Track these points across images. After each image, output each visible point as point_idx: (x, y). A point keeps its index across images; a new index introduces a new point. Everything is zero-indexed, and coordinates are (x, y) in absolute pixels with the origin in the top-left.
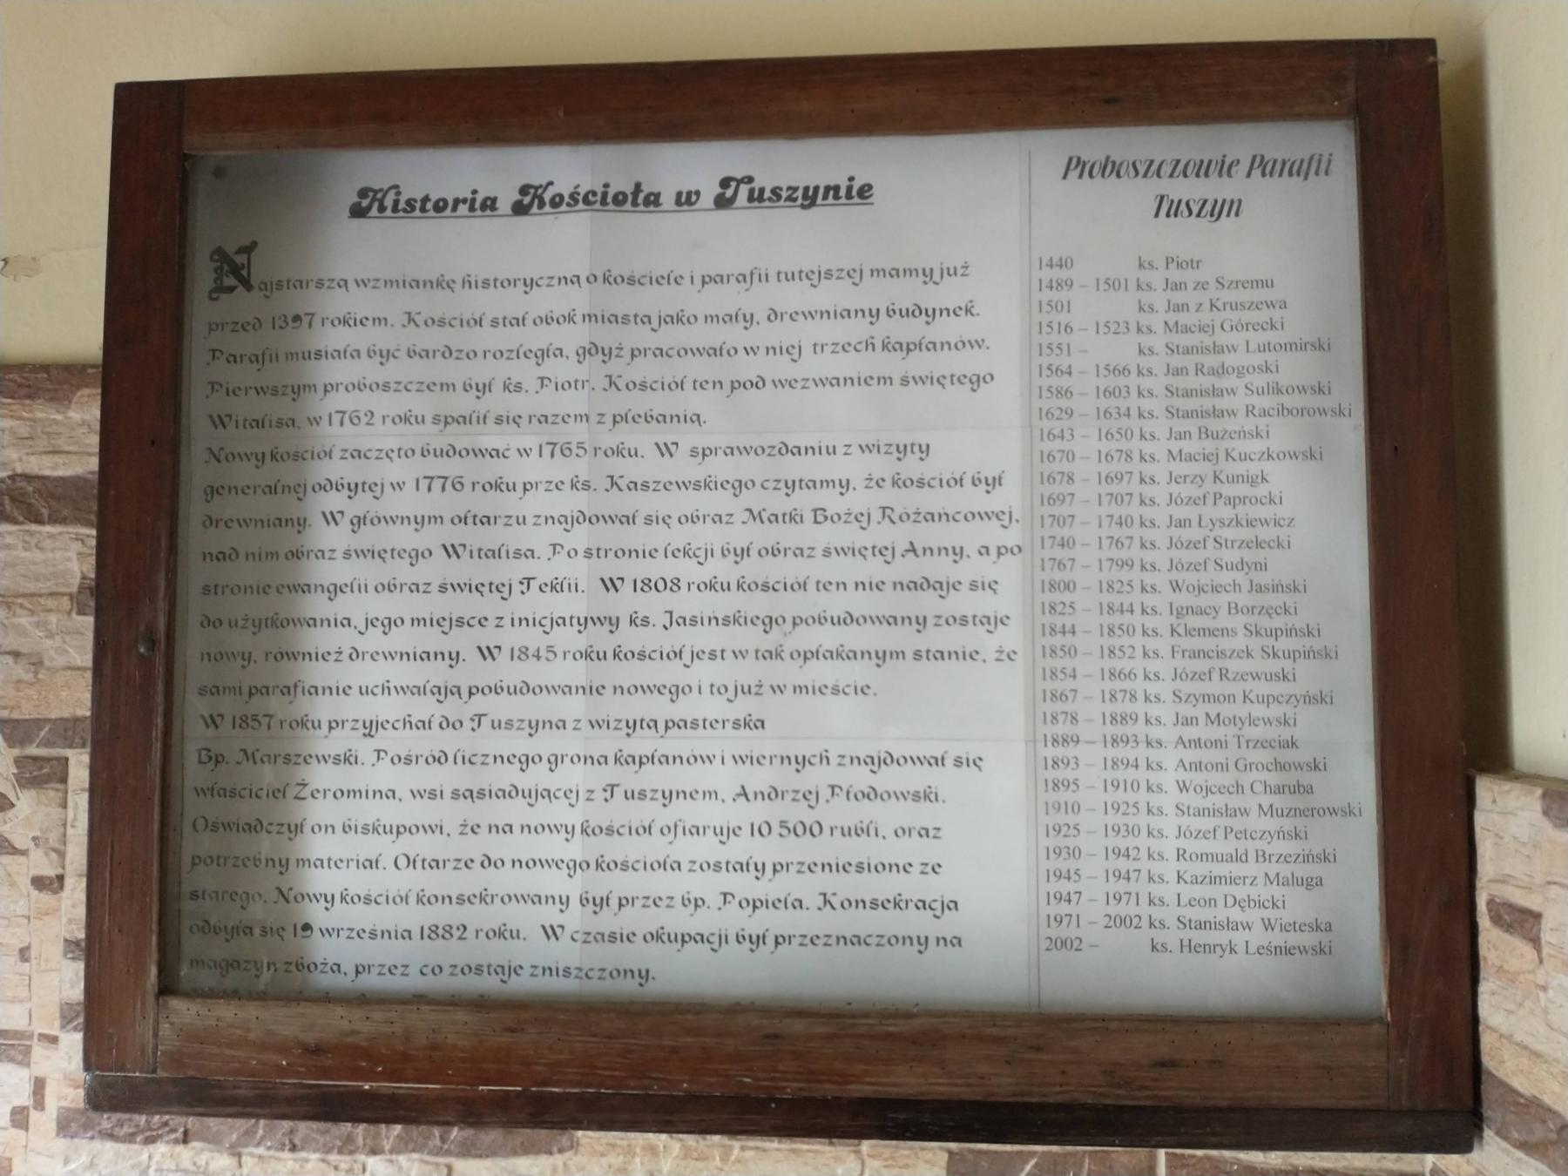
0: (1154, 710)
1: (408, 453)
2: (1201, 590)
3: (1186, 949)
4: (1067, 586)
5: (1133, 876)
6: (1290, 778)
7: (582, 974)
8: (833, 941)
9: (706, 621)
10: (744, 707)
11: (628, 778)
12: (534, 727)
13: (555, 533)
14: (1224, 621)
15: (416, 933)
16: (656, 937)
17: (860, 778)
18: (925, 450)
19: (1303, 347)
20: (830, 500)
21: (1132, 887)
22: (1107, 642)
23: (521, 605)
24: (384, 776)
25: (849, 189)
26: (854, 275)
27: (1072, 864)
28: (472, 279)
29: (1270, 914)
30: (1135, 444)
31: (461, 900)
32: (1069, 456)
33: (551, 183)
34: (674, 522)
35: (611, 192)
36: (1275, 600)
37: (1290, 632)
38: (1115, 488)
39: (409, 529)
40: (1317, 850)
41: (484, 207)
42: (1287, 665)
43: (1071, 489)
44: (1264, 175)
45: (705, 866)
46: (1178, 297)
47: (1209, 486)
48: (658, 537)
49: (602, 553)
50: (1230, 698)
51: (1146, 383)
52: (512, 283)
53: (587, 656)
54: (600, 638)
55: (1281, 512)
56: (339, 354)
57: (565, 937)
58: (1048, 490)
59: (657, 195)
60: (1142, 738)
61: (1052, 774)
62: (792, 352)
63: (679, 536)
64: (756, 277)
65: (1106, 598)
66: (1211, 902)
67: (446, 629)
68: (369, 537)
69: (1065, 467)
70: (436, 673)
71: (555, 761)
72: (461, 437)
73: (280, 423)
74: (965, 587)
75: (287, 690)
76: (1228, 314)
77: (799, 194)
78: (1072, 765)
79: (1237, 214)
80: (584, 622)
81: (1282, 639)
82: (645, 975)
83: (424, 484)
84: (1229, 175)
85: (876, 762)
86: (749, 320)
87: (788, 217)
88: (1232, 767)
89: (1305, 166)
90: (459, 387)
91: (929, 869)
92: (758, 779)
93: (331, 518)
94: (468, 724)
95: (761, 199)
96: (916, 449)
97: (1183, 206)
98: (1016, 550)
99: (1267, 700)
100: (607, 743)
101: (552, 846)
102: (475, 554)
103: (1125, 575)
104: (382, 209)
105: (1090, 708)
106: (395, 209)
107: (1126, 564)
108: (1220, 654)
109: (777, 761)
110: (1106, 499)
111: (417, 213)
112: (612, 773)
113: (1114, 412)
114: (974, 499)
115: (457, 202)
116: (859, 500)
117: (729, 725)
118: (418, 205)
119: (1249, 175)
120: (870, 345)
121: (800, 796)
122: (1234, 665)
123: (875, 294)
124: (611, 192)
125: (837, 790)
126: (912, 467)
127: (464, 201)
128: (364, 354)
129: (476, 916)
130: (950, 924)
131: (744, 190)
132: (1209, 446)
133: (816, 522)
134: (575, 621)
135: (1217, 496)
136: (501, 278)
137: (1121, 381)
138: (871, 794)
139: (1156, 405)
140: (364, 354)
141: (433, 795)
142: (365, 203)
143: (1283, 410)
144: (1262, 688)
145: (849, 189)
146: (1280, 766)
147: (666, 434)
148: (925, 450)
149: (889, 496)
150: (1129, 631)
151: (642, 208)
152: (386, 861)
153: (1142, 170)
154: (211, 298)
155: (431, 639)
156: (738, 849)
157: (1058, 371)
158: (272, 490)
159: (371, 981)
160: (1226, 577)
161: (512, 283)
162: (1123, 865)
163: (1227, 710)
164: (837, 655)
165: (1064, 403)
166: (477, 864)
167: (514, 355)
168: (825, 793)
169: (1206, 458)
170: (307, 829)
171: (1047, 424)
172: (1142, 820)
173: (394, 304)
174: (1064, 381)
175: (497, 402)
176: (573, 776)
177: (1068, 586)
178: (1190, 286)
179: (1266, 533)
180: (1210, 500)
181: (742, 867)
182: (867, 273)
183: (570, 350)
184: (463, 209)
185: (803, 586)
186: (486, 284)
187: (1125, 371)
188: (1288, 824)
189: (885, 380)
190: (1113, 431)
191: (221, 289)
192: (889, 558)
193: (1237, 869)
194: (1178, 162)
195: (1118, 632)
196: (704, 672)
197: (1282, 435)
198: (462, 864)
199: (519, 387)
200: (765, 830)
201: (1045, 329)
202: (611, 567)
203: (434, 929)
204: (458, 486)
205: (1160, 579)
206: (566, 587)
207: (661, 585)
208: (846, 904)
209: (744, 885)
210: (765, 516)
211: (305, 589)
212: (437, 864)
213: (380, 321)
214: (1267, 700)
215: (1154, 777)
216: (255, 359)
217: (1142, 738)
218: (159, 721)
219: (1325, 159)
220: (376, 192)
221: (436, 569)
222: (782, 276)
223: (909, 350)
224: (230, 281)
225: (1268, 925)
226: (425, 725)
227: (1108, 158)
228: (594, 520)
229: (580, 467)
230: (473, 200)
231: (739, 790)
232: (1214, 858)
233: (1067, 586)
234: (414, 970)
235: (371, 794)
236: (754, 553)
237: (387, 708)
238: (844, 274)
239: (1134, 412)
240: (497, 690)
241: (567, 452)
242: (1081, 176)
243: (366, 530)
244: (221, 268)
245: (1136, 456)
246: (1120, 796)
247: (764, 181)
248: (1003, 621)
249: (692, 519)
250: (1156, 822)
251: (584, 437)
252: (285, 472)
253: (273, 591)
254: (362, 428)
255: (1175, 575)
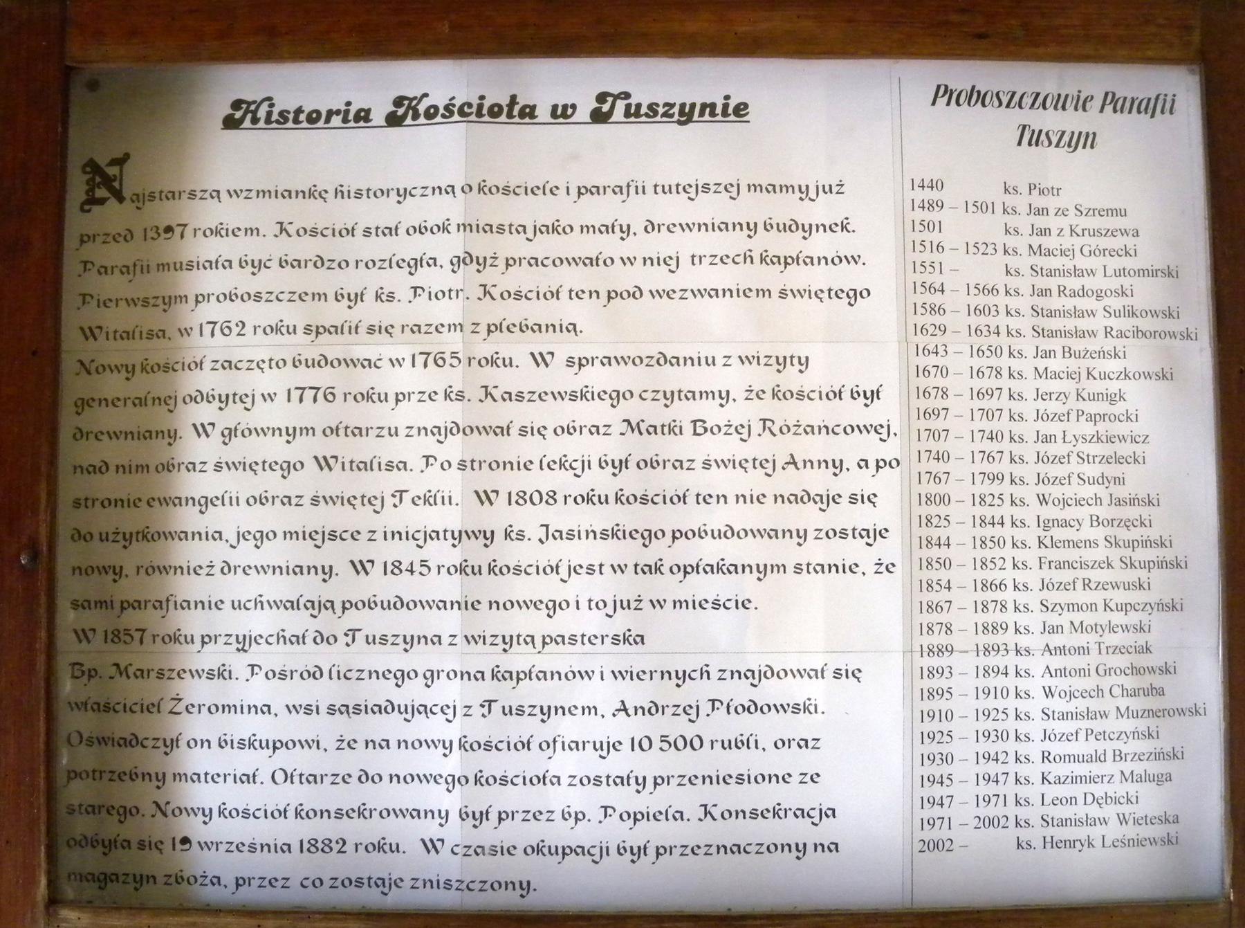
0: (1022, 619)
1: (280, 364)
2: (1066, 503)
3: (1048, 845)
4: (942, 500)
5: (1002, 778)
6: (1145, 681)
7: (464, 886)
8: (713, 850)
9: (583, 535)
10: (622, 622)
11: (506, 693)
12: (410, 642)
13: (428, 444)
14: (1088, 533)
15: (295, 847)
16: (538, 850)
17: (740, 692)
18: (805, 363)
19: (1154, 273)
20: (710, 411)
21: (1000, 789)
22: (980, 553)
23: (394, 518)
24: (258, 690)
25: (726, 106)
26: (731, 190)
27: (945, 770)
28: (345, 189)
29: (1126, 809)
30: (1004, 362)
31: (339, 814)
32: (943, 371)
33: (426, 95)
34: (549, 433)
35: (487, 104)
36: (1132, 512)
37: (1146, 543)
38: (986, 404)
39: (280, 441)
40: (1168, 749)
41: (357, 118)
42: (1143, 574)
43: (945, 404)
44: (1115, 111)
45: (585, 781)
46: (1041, 222)
47: (1073, 404)
48: (530, 448)
49: (476, 465)
50: (1092, 607)
51: (1013, 303)
52: (385, 193)
53: (461, 570)
54: (475, 552)
55: (1137, 428)
56: (211, 265)
57: (445, 851)
58: (923, 404)
59: (533, 108)
60: (1011, 647)
61: (927, 683)
62: (670, 263)
63: (555, 447)
64: (632, 190)
65: (979, 511)
66: (1072, 801)
67: (319, 543)
68: (241, 449)
69: (940, 382)
70: (310, 587)
71: (432, 676)
72: (333, 347)
73: (151, 335)
74: (845, 500)
75: (159, 605)
76: (1087, 240)
77: (676, 110)
78: (946, 674)
79: (1092, 147)
80: (458, 537)
81: (1139, 550)
82: (526, 887)
83: (295, 395)
84: (1084, 110)
85: (753, 676)
86: (626, 231)
87: (667, 133)
88: (1093, 672)
89: (1151, 105)
90: (331, 297)
91: (807, 779)
92: (637, 693)
93: (202, 430)
94: (342, 640)
95: (637, 114)
96: (795, 361)
97: (1043, 137)
98: (894, 463)
99: (1125, 608)
100: (484, 658)
101: (431, 761)
102: (347, 466)
103: (996, 488)
104: (255, 120)
105: (964, 618)
106: (268, 120)
107: (996, 478)
108: (1084, 565)
109: (657, 676)
110: (977, 415)
111: (290, 124)
112: (488, 689)
113: (985, 330)
114: (854, 412)
115: (330, 113)
116: (740, 412)
117: (608, 641)
118: (291, 116)
119: (1101, 111)
120: (748, 258)
121: (680, 711)
122: (1096, 575)
123: (751, 208)
124: (487, 104)
125: (717, 704)
126: (791, 379)
127: (338, 112)
128: (235, 264)
129: (356, 830)
130: (827, 831)
131: (620, 105)
132: (1073, 364)
133: (695, 434)
134: (449, 535)
135: (1080, 413)
136: (374, 188)
137: (990, 300)
138: (753, 708)
139: (1024, 323)
140: (235, 264)
141: (308, 710)
142: (238, 115)
143: (1138, 333)
144: (1120, 597)
145: (726, 106)
146: (1136, 671)
147: (541, 343)
148: (805, 363)
149: (768, 407)
150: (999, 543)
151: (517, 120)
152: (264, 776)
153: (1005, 100)
154: (82, 210)
155: (304, 553)
156: (618, 764)
157: (930, 289)
158: (140, 402)
159: (249, 895)
160: (1087, 491)
161: (385, 193)
162: (992, 768)
163: (1089, 618)
164: (717, 568)
165: (937, 320)
166: (354, 780)
167: (386, 264)
168: (706, 708)
169: (1070, 376)
170: (183, 743)
171: (922, 340)
172: (1011, 725)
173: (266, 213)
174: (937, 299)
175: (369, 312)
176: (448, 692)
177: (944, 500)
178: (1052, 212)
179: (1125, 449)
180: (1073, 416)
181: (623, 781)
182: (744, 189)
183: (444, 260)
184: (336, 121)
185: (683, 499)
186: (359, 195)
187: (993, 290)
188: (1142, 725)
189: (764, 293)
190: (984, 348)
191: (93, 200)
192: (770, 471)
193: (1096, 769)
194: (1038, 94)
195: (990, 544)
196: (581, 587)
197: (1139, 356)
198: (339, 779)
199: (391, 297)
200: (645, 744)
201: (919, 248)
202: (486, 480)
203: (313, 843)
204: (330, 397)
205: (1029, 493)
206: (439, 500)
207: (536, 498)
208: (726, 815)
209: (625, 799)
210: (643, 427)
211: (178, 501)
212: (314, 779)
213: (252, 231)
214: (1125, 608)
215: (1023, 684)
216: (125, 270)
217: (1011, 647)
218: (43, 634)
219: (1169, 99)
220: (249, 104)
221: (307, 481)
222: (659, 189)
223: (786, 264)
224: (101, 193)
225: (1123, 820)
226: (299, 639)
227: (973, 87)
228: (468, 431)
229: (454, 377)
230: (347, 112)
231: (619, 706)
232: (1076, 759)
233: (942, 500)
234: (294, 883)
235: (246, 710)
236: (632, 464)
237: (261, 622)
238: (721, 188)
239: (1003, 331)
240: (370, 605)
241: (440, 362)
242: (948, 103)
243: (237, 441)
244: (93, 179)
245: (1005, 373)
246: (990, 703)
247: (641, 97)
248: (882, 534)
249: (568, 430)
250: (1023, 727)
251: (458, 347)
252: (157, 384)
253: (143, 504)
254: (233, 339)
255: (1042, 489)
